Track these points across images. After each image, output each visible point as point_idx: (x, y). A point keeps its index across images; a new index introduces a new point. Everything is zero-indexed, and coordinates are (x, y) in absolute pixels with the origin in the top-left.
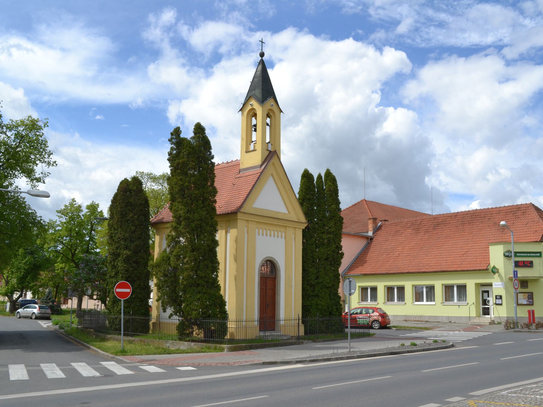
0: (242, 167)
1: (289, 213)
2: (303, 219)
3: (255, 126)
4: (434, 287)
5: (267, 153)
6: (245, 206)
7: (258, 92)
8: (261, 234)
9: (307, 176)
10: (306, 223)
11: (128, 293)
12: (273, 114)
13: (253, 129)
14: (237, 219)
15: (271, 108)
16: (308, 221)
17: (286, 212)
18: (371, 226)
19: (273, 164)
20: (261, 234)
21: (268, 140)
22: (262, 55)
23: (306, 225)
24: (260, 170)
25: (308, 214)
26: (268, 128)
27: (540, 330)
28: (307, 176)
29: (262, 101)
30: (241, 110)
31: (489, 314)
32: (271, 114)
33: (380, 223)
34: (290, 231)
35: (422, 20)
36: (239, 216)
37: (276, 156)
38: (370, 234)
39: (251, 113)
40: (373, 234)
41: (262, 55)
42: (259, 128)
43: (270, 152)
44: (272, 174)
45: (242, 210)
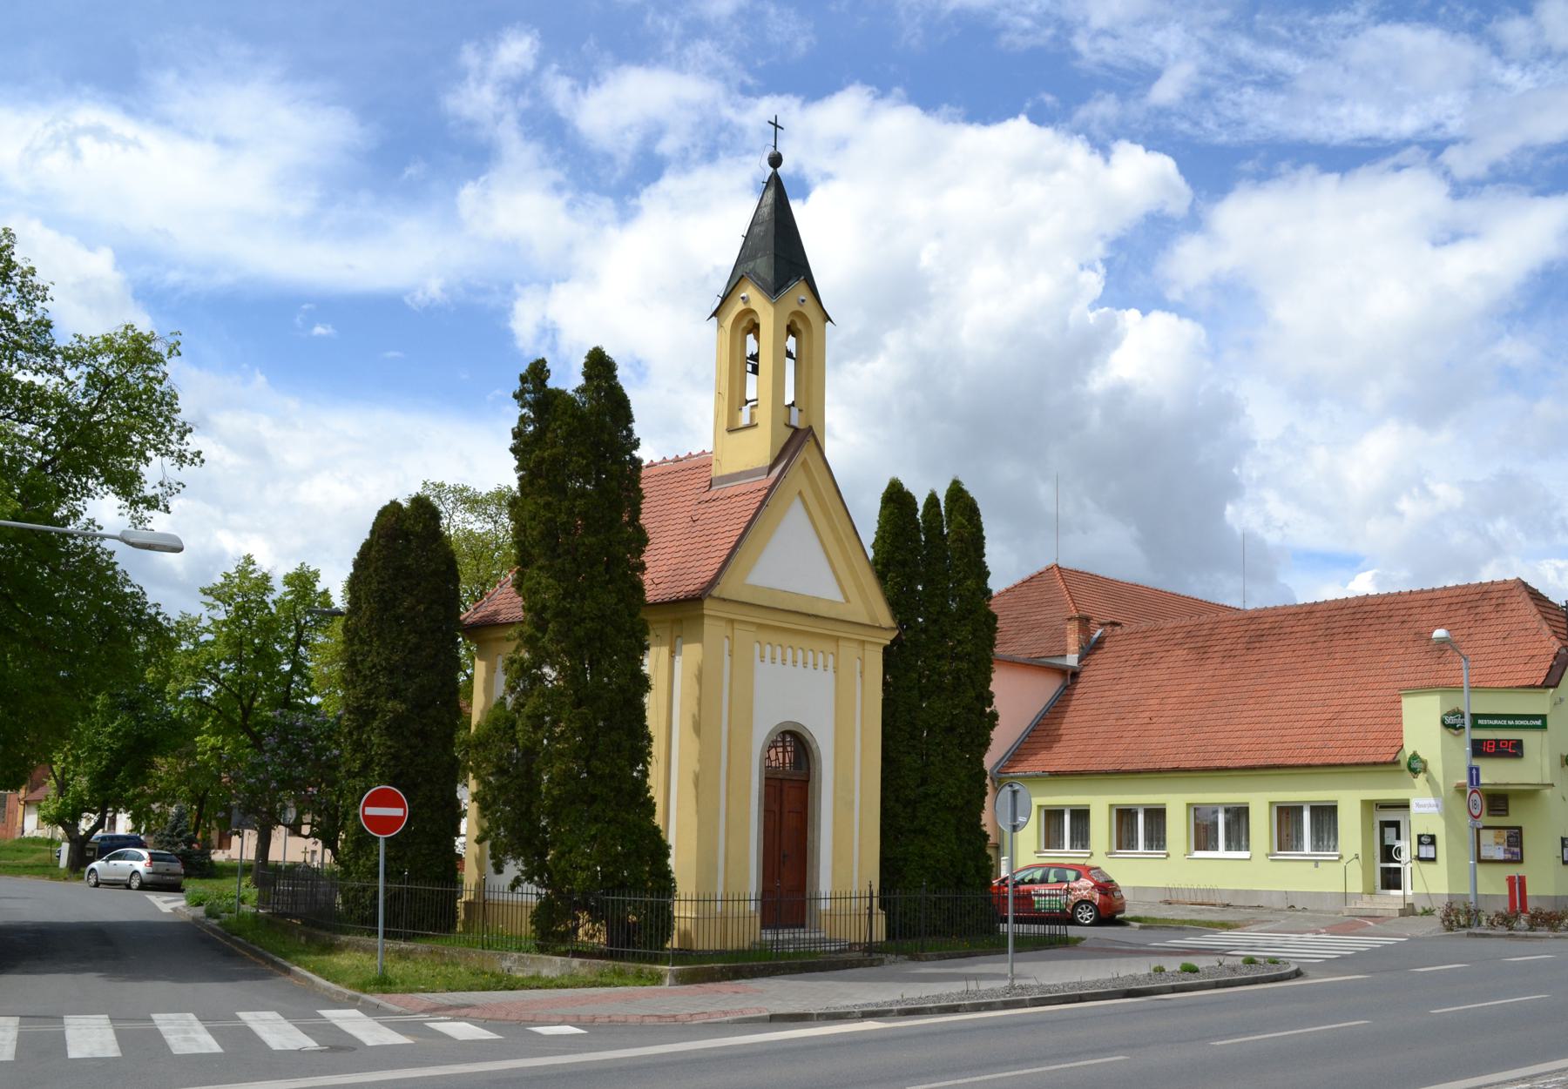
1: (848, 601)
2: (884, 616)
5: (788, 433)
6: (723, 580)
7: (764, 265)
10: (892, 629)
11: (398, 820)
12: (806, 327)
13: (749, 368)
16: (900, 624)
17: (839, 598)
19: (804, 463)
22: (776, 161)
26: (790, 363)
29: (775, 289)
32: (800, 325)
34: (849, 651)
36: (709, 607)
38: (1072, 660)
39: (744, 324)
40: (1080, 660)
41: (776, 161)
42: (766, 363)
43: (796, 430)
44: (800, 493)
45: (716, 592)
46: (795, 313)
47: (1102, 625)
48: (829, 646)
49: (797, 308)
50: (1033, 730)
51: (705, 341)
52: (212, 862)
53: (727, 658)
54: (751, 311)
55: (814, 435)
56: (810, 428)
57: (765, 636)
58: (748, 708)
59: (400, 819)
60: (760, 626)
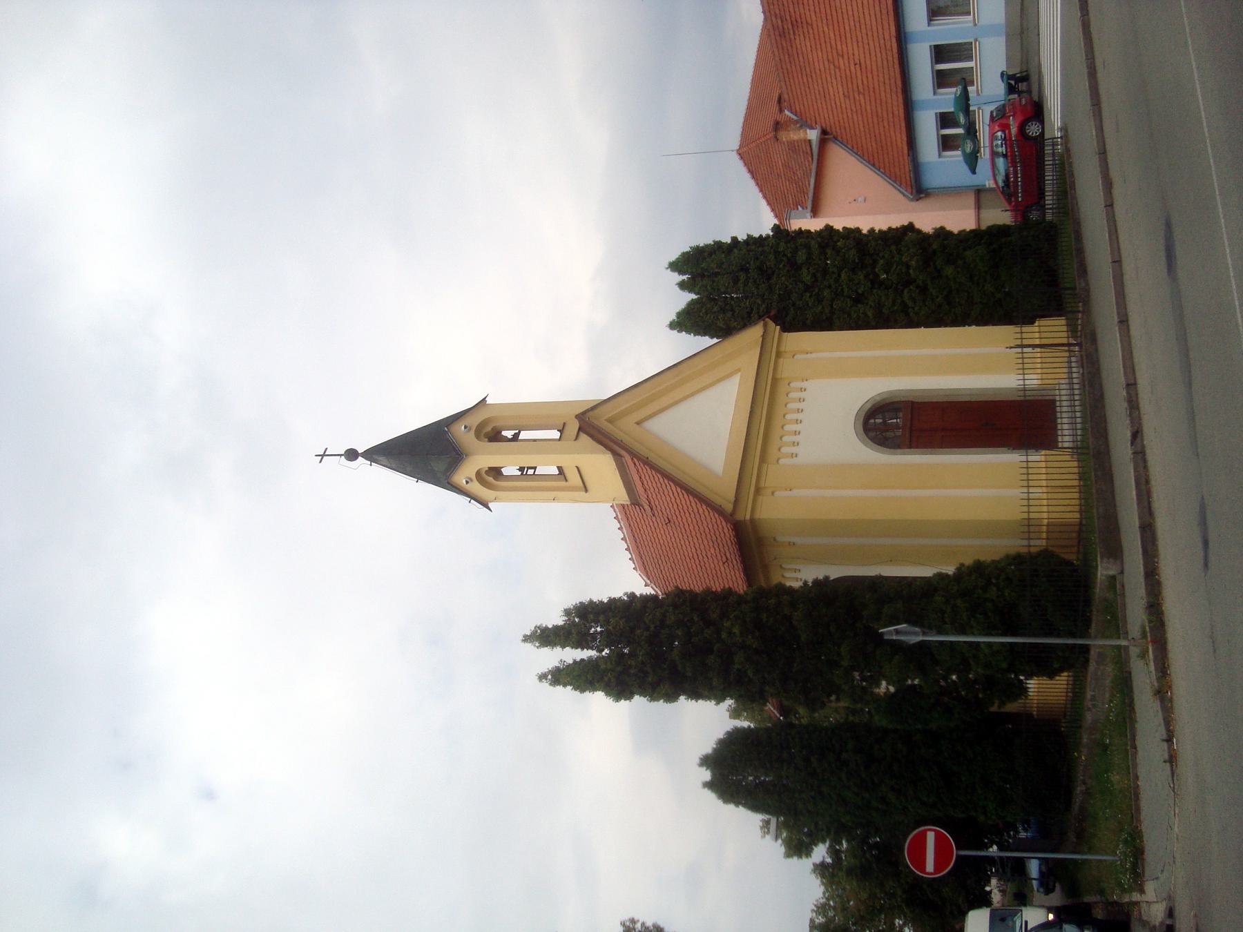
0: (624, 498)
1: (739, 370)
2: (754, 333)
3: (521, 469)
4: (936, 47)
5: (583, 437)
6: (718, 501)
7: (439, 466)
8: (794, 450)
9: (688, 321)
10: (765, 326)
11: (939, 837)
12: (491, 426)
13: (531, 472)
14: (752, 520)
15: (473, 432)
16: (760, 317)
17: (736, 379)
18: (795, 135)
19: (610, 421)
20: (794, 450)
21: (555, 434)
22: (352, 455)
23: (771, 324)
24: (627, 458)
25: (746, 321)
26: (524, 435)
27: (621, 929)
28: (688, 321)
29: (456, 456)
30: (485, 505)
31: (968, 13)
32: (489, 429)
33: (787, 112)
34: (788, 368)
35: (770, 271)
36: (745, 515)
37: (591, 413)
38: (813, 135)
39: (490, 479)
40: (812, 128)
41: (352, 455)
42: (526, 461)
43: (580, 429)
44: (638, 423)
45: (729, 508)
46: (478, 436)
47: (781, 111)
48: (782, 389)
49: (472, 434)
50: (873, 165)
51: (515, 514)
52: (963, 915)
53: (814, 355)
54: (478, 474)
55: (584, 413)
56: (577, 417)
57: (773, 451)
58: (837, 449)
59: (938, 835)
60: (763, 459)
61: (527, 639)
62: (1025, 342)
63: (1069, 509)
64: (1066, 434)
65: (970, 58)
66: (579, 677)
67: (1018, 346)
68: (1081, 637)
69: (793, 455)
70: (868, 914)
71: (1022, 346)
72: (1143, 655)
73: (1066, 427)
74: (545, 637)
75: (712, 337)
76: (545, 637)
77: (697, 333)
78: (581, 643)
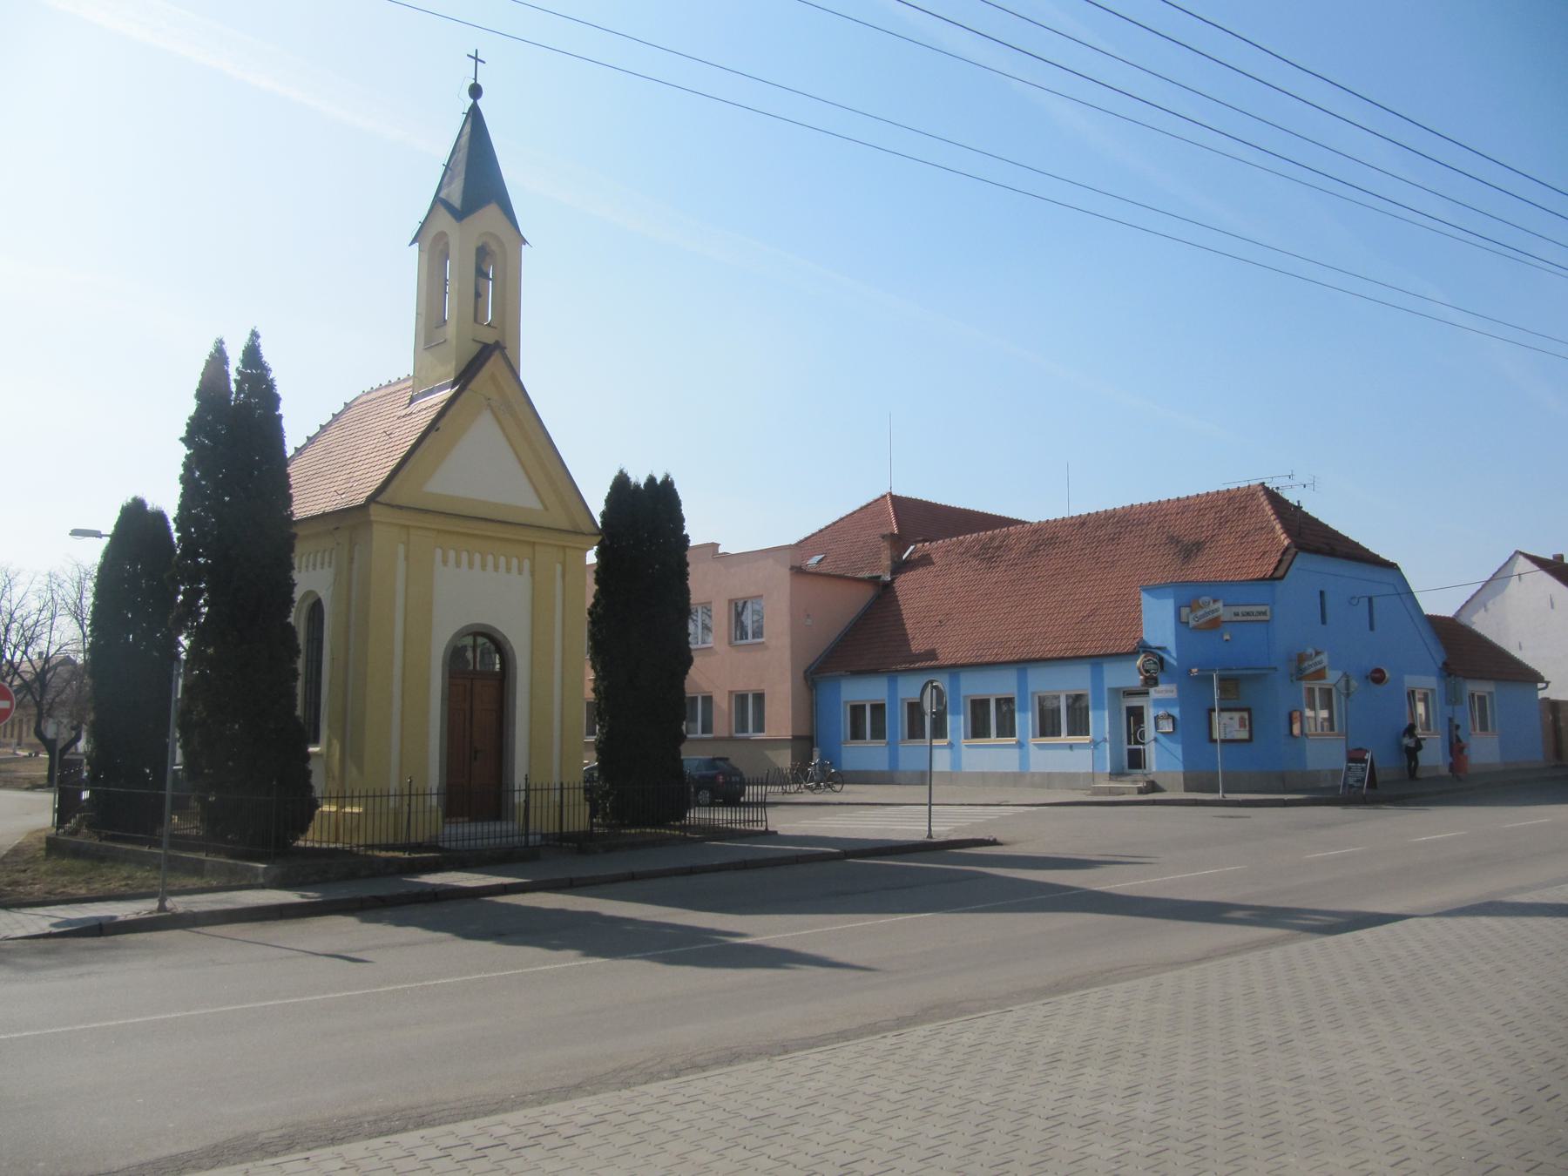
5: (479, 346)
22: (476, 91)
41: (476, 91)
61: (255, 335)
62: (532, 794)
63: (391, 831)
64: (466, 832)
65: (873, 737)
66: (211, 391)
67: (527, 786)
68: (998, 728)
69: (445, 562)
70: (40, 688)
71: (562, 789)
72: (1236, 614)
73: (473, 829)
74: (252, 355)
75: (604, 515)
76: (252, 355)
77: (609, 500)
78: (244, 378)
